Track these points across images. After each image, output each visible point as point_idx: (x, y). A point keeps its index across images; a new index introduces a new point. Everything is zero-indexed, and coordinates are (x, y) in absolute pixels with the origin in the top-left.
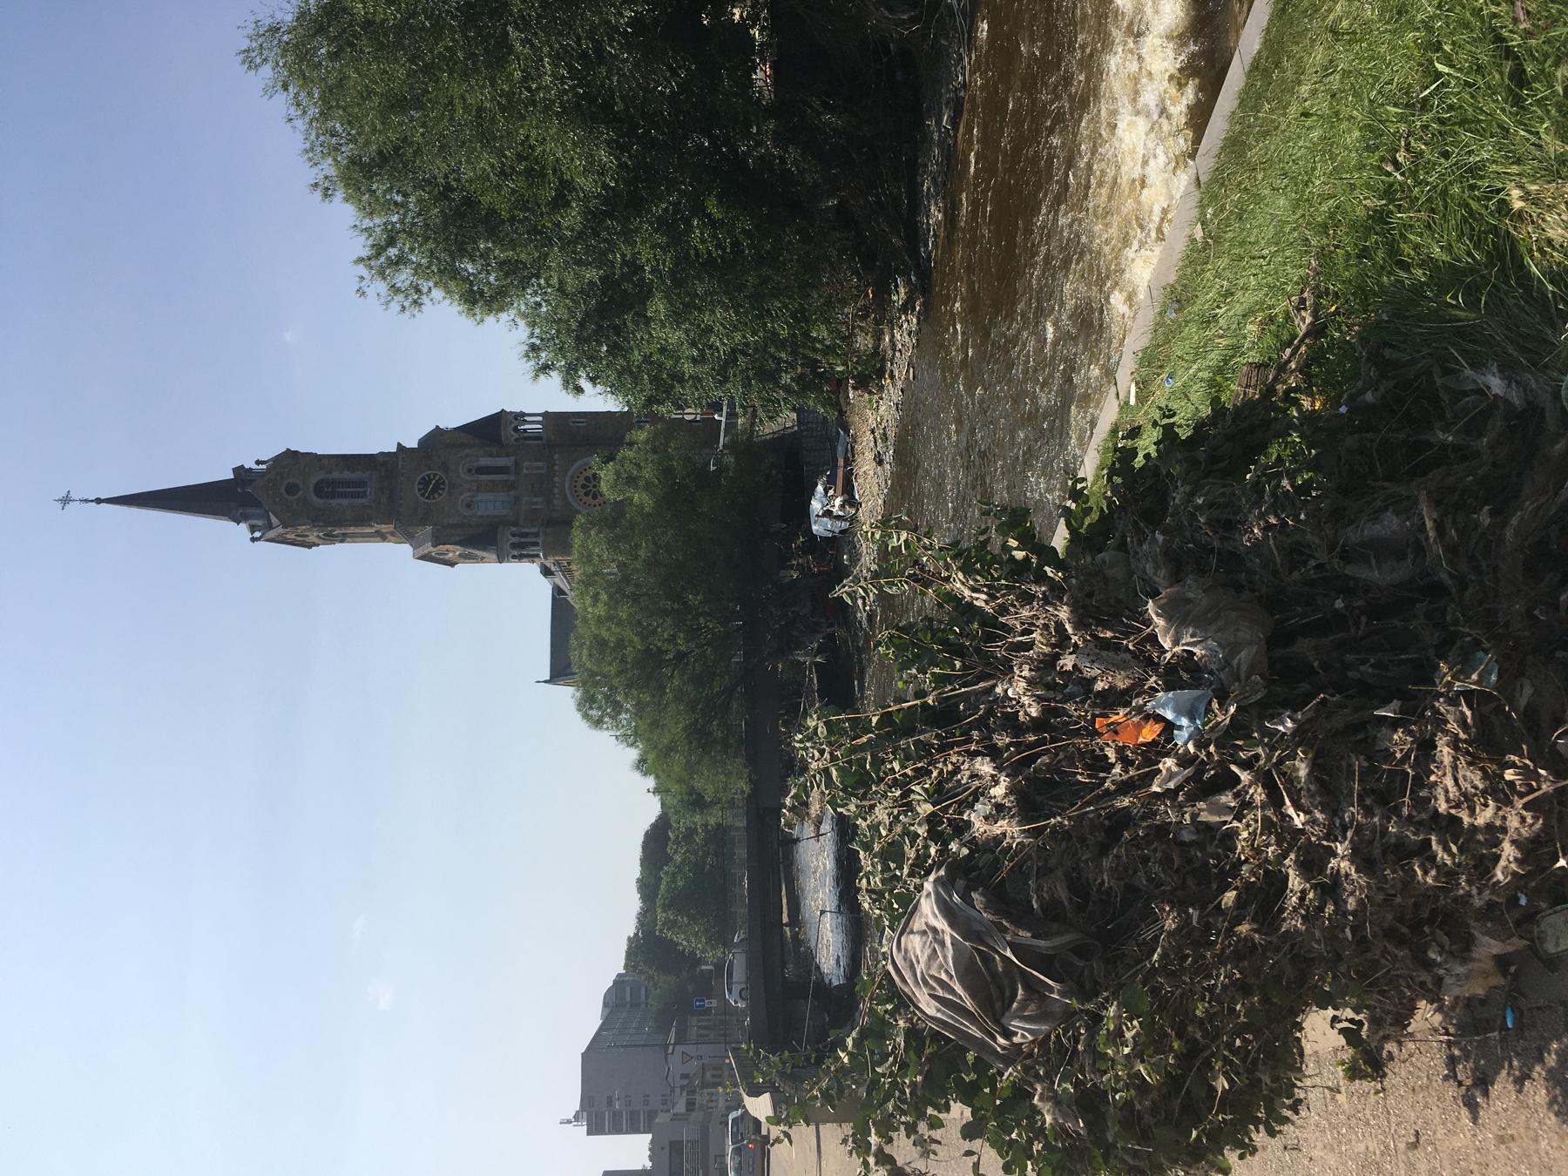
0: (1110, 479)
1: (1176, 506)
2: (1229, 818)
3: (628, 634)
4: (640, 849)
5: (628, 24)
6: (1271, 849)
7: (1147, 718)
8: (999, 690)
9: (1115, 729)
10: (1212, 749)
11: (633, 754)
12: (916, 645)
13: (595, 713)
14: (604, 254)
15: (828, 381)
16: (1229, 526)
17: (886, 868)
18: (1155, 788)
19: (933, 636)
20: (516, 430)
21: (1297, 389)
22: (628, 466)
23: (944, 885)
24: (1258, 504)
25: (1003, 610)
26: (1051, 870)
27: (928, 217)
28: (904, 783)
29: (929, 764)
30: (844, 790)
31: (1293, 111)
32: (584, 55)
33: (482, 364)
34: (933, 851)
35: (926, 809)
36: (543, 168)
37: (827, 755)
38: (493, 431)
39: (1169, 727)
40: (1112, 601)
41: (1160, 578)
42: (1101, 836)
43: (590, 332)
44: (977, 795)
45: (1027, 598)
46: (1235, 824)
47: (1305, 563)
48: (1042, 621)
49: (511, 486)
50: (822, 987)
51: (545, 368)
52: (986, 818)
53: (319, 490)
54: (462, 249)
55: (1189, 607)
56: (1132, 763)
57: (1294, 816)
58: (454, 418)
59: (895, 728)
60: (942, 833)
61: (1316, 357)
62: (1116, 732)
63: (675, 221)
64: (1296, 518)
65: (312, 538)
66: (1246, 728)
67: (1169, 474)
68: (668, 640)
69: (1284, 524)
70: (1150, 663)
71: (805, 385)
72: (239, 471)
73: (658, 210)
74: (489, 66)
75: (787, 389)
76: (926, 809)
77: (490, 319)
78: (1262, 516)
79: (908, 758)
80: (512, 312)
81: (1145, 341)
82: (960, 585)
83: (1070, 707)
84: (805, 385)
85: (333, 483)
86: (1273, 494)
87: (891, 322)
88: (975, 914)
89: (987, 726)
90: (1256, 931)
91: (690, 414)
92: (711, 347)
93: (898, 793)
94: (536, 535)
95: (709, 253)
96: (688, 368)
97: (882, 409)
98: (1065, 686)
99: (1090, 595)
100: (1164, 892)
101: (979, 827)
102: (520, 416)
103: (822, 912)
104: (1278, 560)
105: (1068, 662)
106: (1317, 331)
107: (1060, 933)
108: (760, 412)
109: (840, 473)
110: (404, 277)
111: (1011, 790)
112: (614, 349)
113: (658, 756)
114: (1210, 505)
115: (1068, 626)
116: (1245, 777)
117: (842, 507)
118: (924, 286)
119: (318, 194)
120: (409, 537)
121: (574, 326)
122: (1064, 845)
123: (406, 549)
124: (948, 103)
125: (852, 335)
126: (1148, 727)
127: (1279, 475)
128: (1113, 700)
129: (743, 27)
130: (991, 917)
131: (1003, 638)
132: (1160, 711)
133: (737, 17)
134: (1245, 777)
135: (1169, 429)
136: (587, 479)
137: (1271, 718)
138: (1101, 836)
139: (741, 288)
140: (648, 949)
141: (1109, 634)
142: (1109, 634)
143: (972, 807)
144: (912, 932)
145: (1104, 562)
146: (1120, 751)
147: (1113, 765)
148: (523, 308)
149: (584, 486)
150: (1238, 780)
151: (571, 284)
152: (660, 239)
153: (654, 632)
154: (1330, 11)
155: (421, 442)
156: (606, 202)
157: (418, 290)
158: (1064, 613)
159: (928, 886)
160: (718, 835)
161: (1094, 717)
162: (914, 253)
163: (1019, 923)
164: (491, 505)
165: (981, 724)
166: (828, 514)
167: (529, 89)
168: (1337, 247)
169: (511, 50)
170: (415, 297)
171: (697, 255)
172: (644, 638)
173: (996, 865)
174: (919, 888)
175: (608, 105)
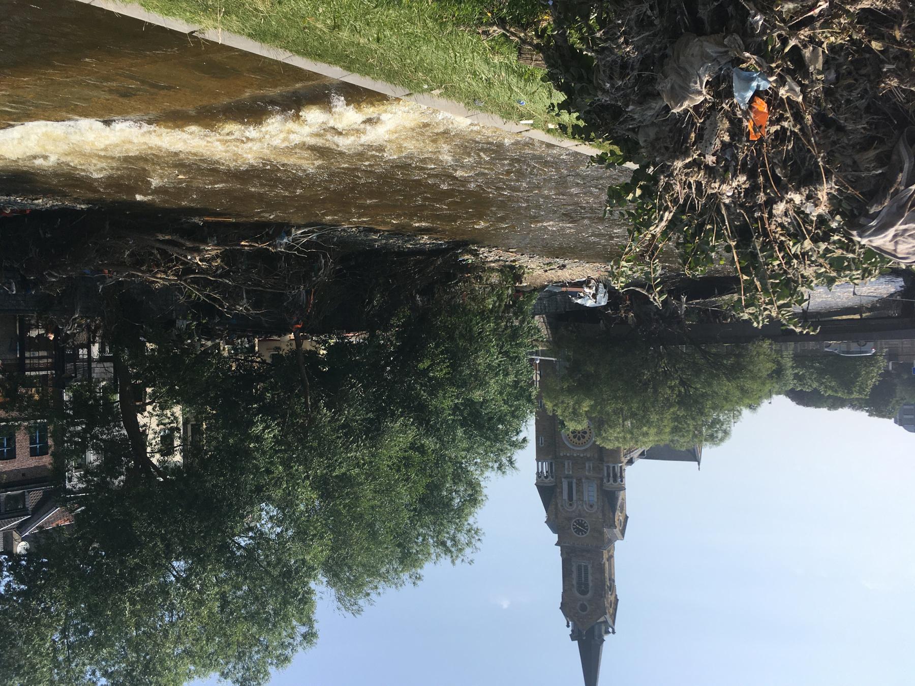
0: (592, 140)
1: (610, 100)
2: (820, 49)
3: (668, 416)
4: (809, 408)
5: (330, 411)
6: (842, 21)
7: (751, 107)
8: (727, 201)
9: (757, 127)
10: (773, 65)
11: (746, 412)
12: (696, 251)
13: (720, 435)
14: (448, 426)
15: (518, 298)
16: (624, 66)
17: (849, 268)
18: (800, 99)
19: (689, 242)
20: (546, 477)
21: (536, 31)
22: (566, 414)
23: (864, 231)
24: (611, 50)
25: (675, 201)
26: (855, 162)
27: (426, 244)
28: (789, 258)
29: (776, 242)
30: (792, 295)
31: (374, 46)
32: (346, 434)
33: (510, 495)
34: (836, 238)
35: (808, 244)
36: (404, 458)
37: (768, 307)
38: (548, 491)
39: (758, 93)
40: (671, 135)
41: (657, 106)
42: (831, 132)
43: (489, 430)
44: (799, 211)
45: (668, 187)
46: (825, 45)
47: (649, 17)
48: (682, 177)
49: (579, 481)
50: (905, 292)
51: (511, 462)
52: (816, 206)
53: (584, 593)
54: (446, 505)
55: (677, 87)
56: (782, 115)
57: (820, 8)
58: (541, 513)
59: (751, 263)
60: (824, 232)
61: (517, 22)
62: (761, 127)
63: (430, 386)
64: (620, 26)
65: (612, 598)
66: (760, 44)
67: (590, 105)
68: (673, 391)
69: (624, 33)
70: (713, 108)
71: (519, 312)
72: (573, 637)
73: (425, 395)
74: (352, 486)
75: (522, 322)
76: (808, 244)
77: (485, 491)
78: (619, 47)
79: (771, 256)
80: (480, 478)
81: (497, 117)
82: (657, 229)
83: (741, 156)
84: (519, 312)
85: (579, 584)
86: (605, 41)
87: (483, 263)
88: (885, 210)
89: (752, 207)
90: (900, 26)
91: (536, 376)
92: (499, 365)
93: (795, 261)
94: (608, 467)
95: (448, 367)
96: (511, 379)
97: (533, 266)
98: (726, 160)
99: (667, 148)
100: (872, 88)
101: (822, 209)
102: (539, 475)
103: (854, 294)
104: (647, 34)
105: (710, 159)
106: (502, 23)
107: (899, 156)
108: (535, 337)
109: (570, 289)
110: (462, 538)
111: (797, 190)
112: (501, 420)
113: (747, 398)
114: (611, 78)
115: (687, 161)
116: (793, 42)
117: (590, 288)
118: (464, 245)
119: (418, 582)
120: (611, 542)
121: (488, 443)
122: (836, 155)
123: (618, 544)
124: (366, 236)
125: (491, 285)
126: (756, 107)
127: (593, 39)
128: (737, 130)
129: (329, 349)
130: (888, 200)
131: (693, 200)
132: (747, 100)
133: (325, 352)
134: (793, 42)
135: (562, 106)
136: (575, 437)
137: (753, 29)
138: (831, 132)
139: (465, 350)
140: (878, 403)
141: (693, 135)
142: (693, 135)
143: (808, 215)
144: (895, 250)
145: (645, 141)
146: (772, 123)
147: (782, 127)
148: (477, 472)
149: (579, 439)
150: (795, 47)
151: (465, 445)
152: (441, 393)
153: (668, 399)
154: (321, 30)
155: (554, 531)
156: (421, 424)
157: (469, 531)
158: (679, 164)
159: (864, 241)
160: (800, 359)
161: (748, 141)
162: (446, 251)
163: (892, 182)
164: (591, 493)
165: (750, 211)
166: (594, 296)
167: (364, 464)
168: (454, 16)
169: (344, 474)
170: (473, 532)
171: (448, 373)
172: (671, 406)
173: (850, 198)
174: (863, 247)
175: (371, 421)
